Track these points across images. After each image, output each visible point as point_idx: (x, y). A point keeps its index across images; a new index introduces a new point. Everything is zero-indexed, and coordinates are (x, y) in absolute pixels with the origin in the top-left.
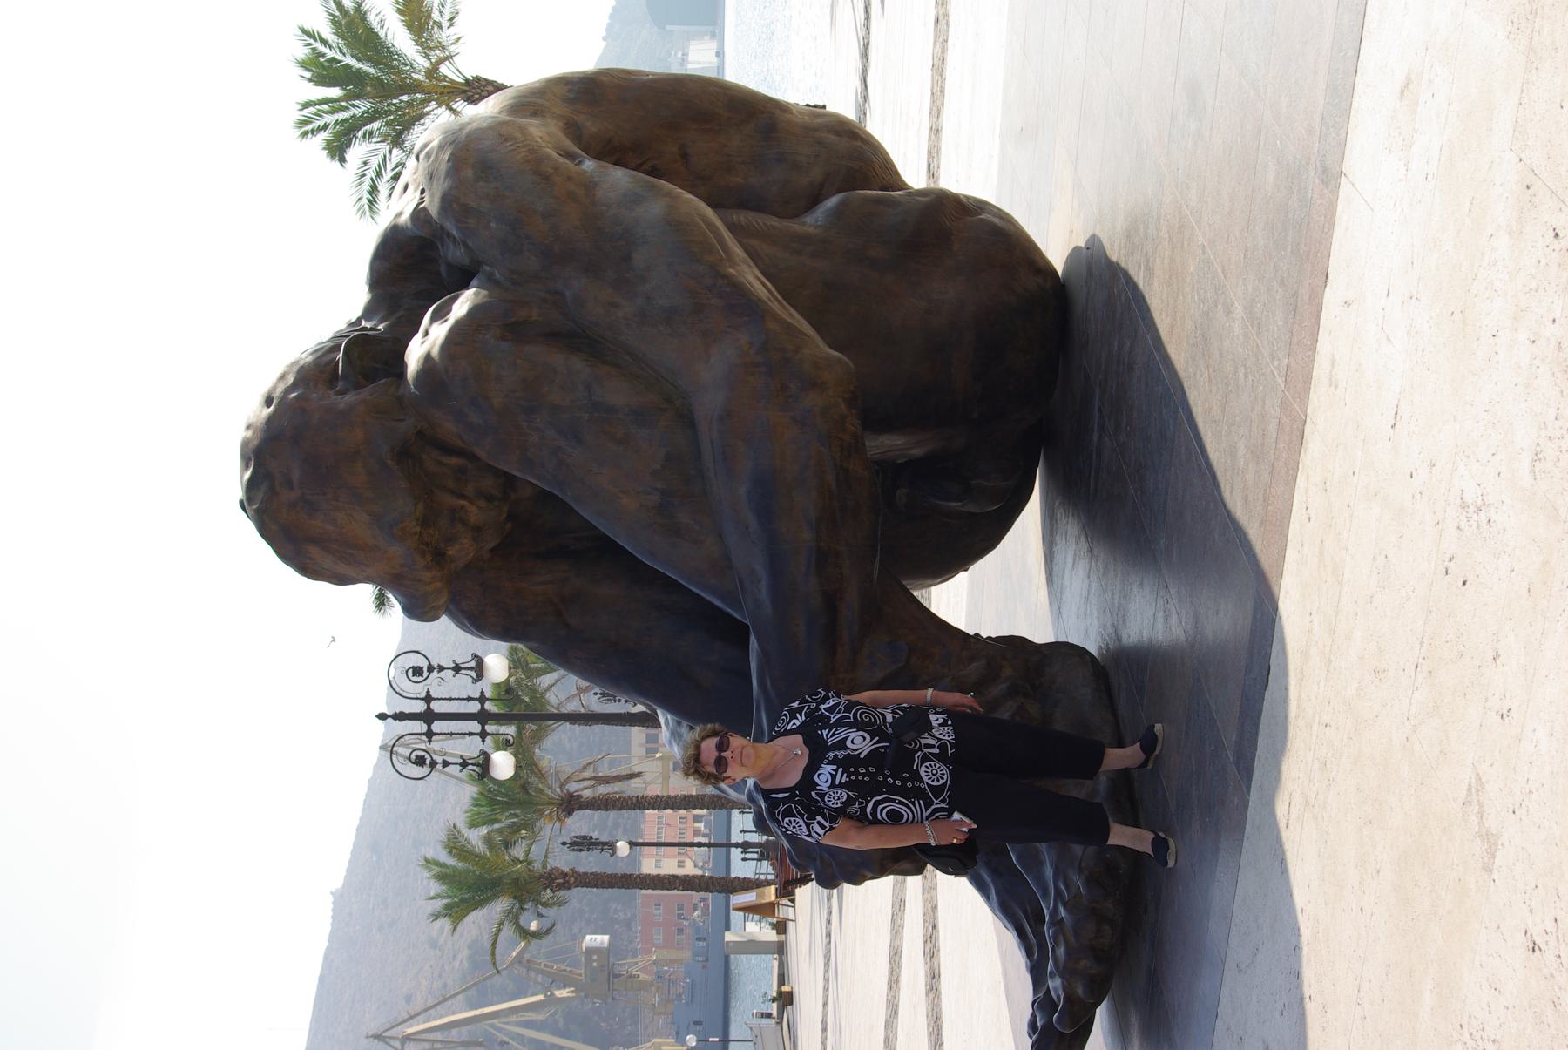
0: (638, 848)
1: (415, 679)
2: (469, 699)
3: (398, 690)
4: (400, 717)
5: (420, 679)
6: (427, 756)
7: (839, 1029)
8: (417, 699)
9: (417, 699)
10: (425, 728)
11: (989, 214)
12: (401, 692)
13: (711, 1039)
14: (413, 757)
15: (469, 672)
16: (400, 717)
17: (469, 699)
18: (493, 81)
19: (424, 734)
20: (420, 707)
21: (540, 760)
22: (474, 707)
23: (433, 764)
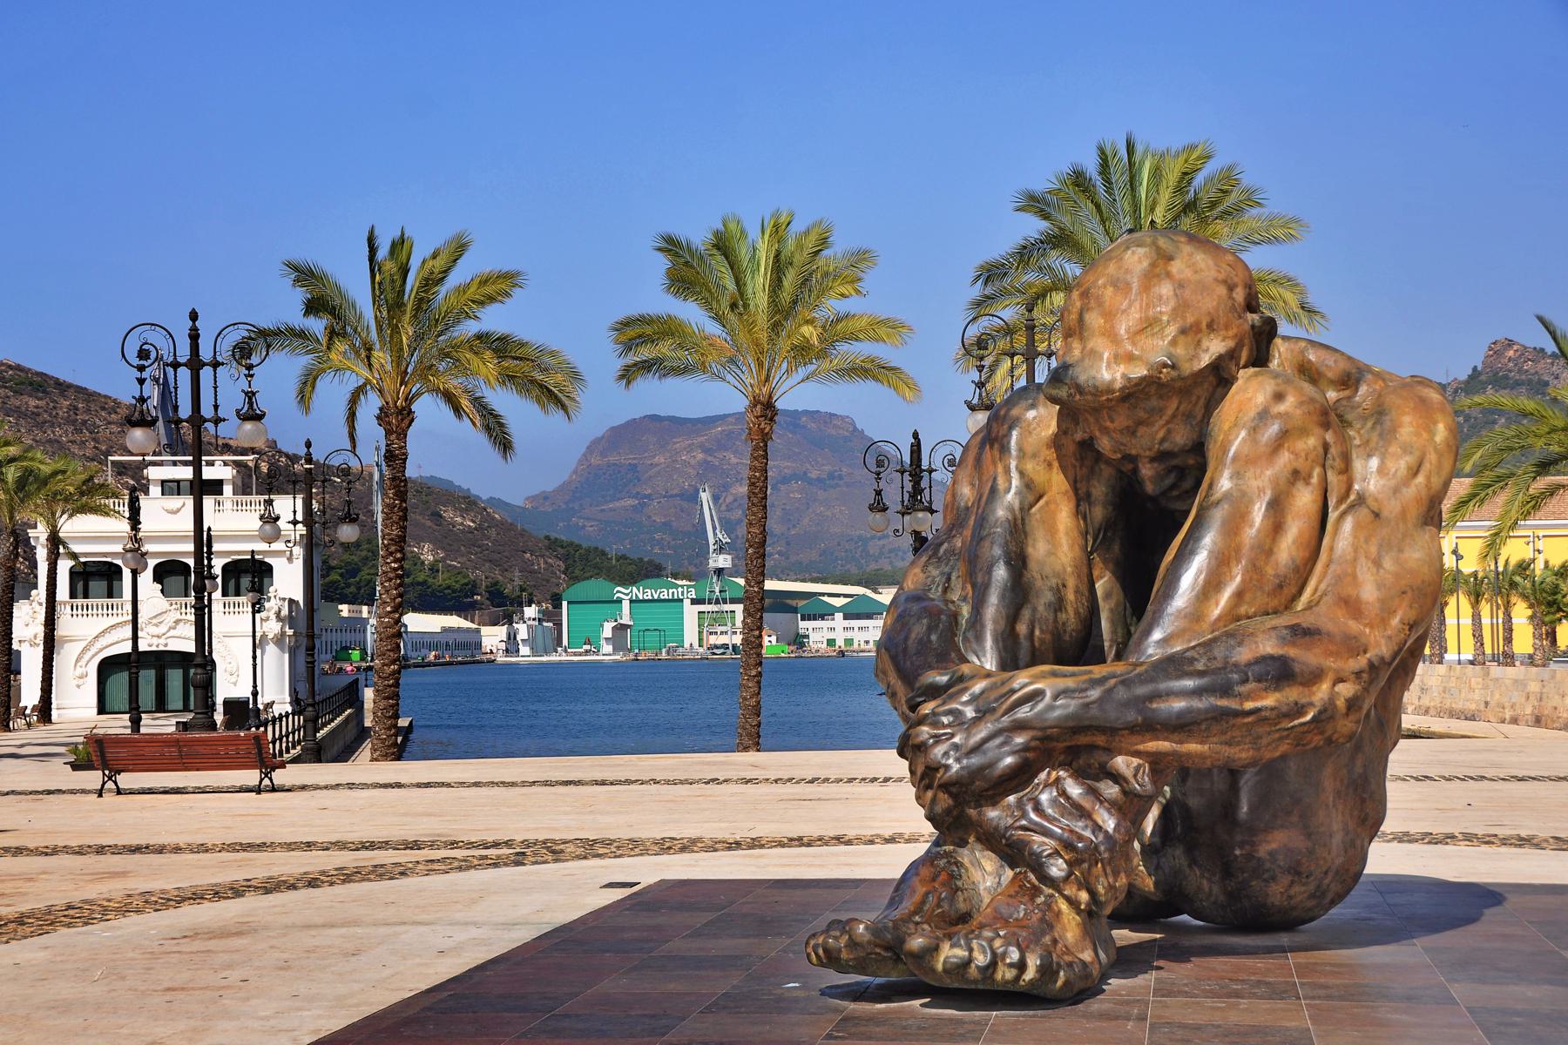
0: (193, 618)
1: (946, 461)
2: (216, 407)
3: (224, 332)
4: (194, 336)
5: (946, 465)
6: (150, 362)
7: (1551, 324)
8: (215, 352)
9: (215, 352)
10: (182, 360)
11: (1007, 854)
12: (222, 336)
13: (551, 624)
14: (145, 347)
15: (246, 406)
16: (194, 336)
17: (216, 407)
18: (542, 350)
19: (175, 358)
20: (206, 354)
21: (1067, 492)
22: (207, 411)
23: (141, 369)
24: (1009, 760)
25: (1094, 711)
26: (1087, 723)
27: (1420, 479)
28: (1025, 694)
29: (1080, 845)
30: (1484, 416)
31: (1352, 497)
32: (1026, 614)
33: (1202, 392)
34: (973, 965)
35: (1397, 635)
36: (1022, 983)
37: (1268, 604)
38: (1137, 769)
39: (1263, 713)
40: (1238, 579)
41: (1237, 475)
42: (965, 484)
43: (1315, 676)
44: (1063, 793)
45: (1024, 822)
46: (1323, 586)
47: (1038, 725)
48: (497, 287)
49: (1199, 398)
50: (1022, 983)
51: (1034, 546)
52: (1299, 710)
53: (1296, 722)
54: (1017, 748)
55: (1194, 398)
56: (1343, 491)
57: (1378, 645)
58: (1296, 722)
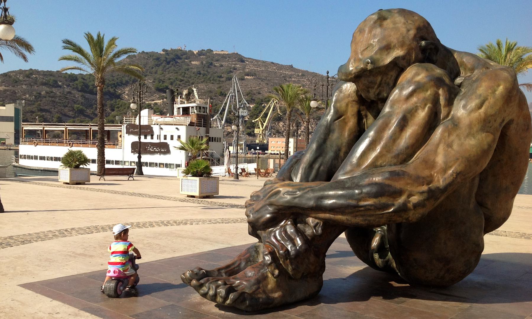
24: (268, 216)
25: (296, 200)
26: (293, 205)
27: (482, 110)
28: (274, 192)
29: (281, 252)
30: (23, 78)
31: (450, 117)
32: (320, 160)
33: (393, 74)
34: (208, 294)
35: (449, 178)
36: (226, 304)
37: (391, 161)
38: (317, 224)
39: (367, 207)
40: (379, 151)
41: (392, 107)
42: (390, 110)
43: (399, 193)
44: (286, 232)
45: (268, 240)
46: (419, 155)
47: (276, 204)
48: (113, 41)
49: (392, 76)
50: (226, 304)
51: (332, 136)
52: (388, 206)
53: (385, 212)
54: (270, 212)
55: (389, 77)
56: (445, 114)
57: (438, 181)
58: (385, 212)
